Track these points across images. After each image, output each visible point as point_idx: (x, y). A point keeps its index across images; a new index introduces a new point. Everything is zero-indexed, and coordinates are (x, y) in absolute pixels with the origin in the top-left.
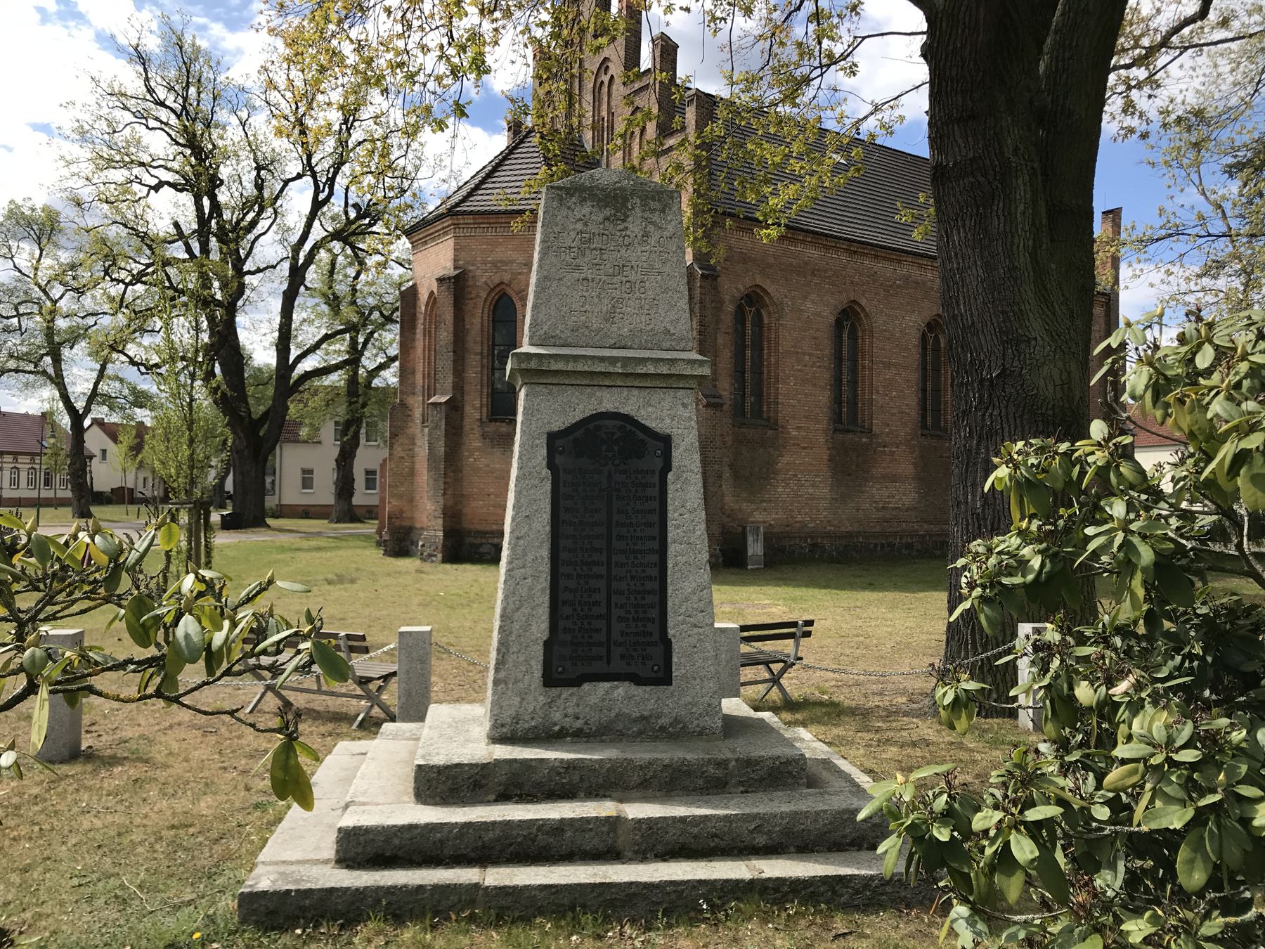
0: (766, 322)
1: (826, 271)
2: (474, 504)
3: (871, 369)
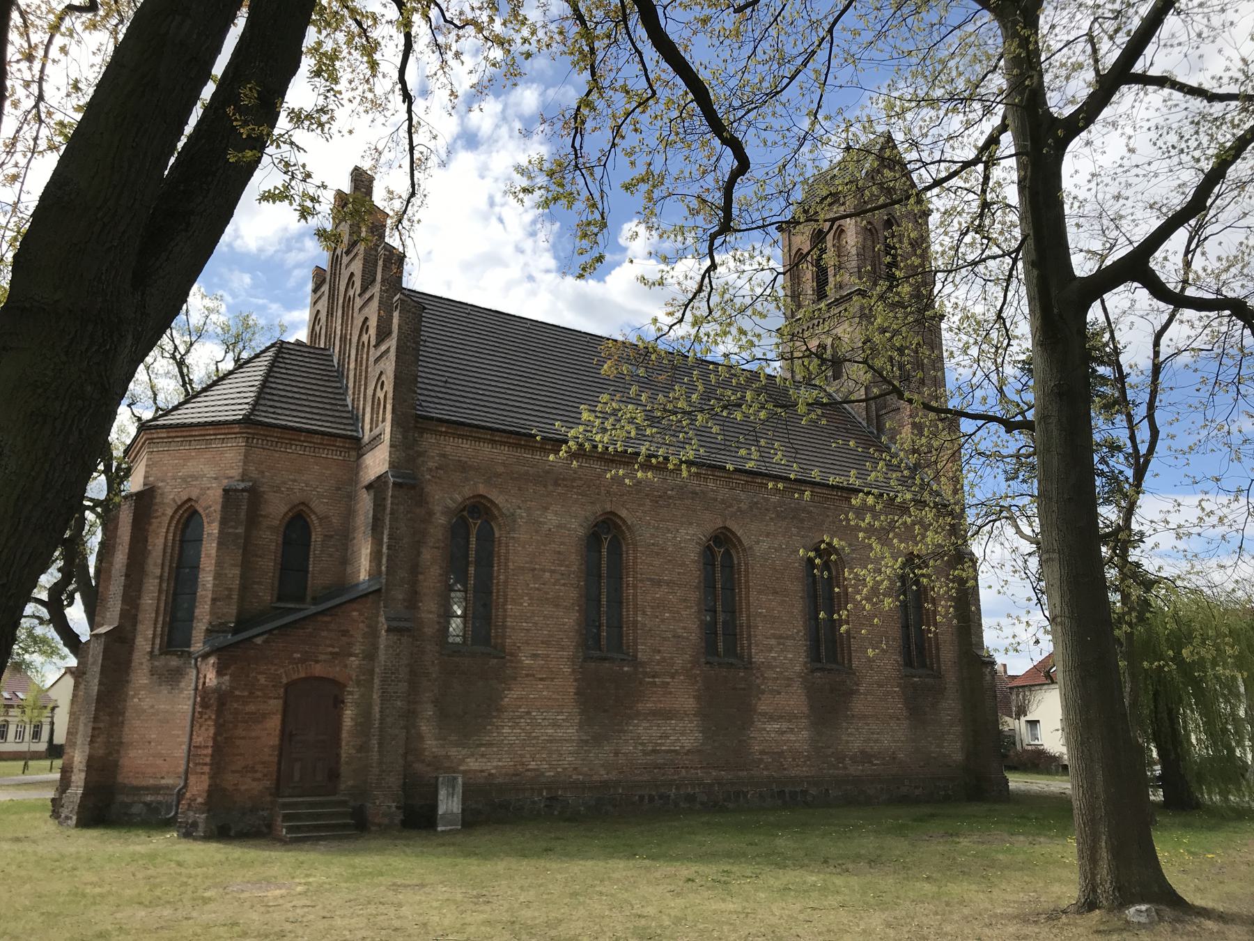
0: (497, 535)
1: (574, 480)
2: (132, 753)
3: (635, 587)
